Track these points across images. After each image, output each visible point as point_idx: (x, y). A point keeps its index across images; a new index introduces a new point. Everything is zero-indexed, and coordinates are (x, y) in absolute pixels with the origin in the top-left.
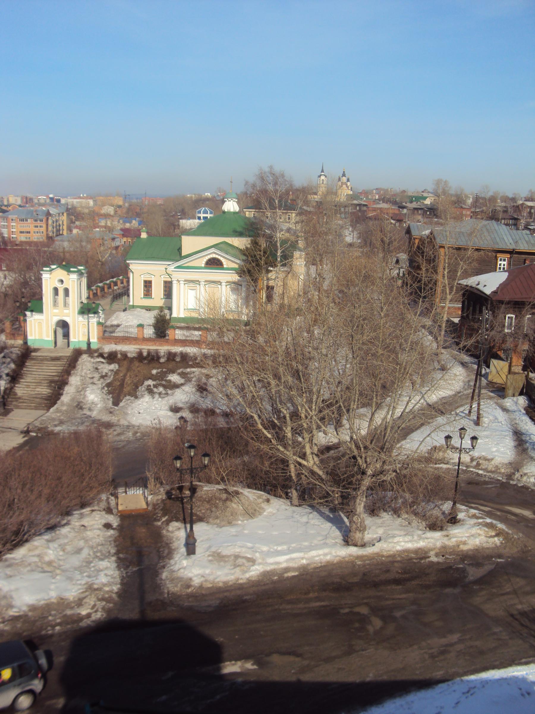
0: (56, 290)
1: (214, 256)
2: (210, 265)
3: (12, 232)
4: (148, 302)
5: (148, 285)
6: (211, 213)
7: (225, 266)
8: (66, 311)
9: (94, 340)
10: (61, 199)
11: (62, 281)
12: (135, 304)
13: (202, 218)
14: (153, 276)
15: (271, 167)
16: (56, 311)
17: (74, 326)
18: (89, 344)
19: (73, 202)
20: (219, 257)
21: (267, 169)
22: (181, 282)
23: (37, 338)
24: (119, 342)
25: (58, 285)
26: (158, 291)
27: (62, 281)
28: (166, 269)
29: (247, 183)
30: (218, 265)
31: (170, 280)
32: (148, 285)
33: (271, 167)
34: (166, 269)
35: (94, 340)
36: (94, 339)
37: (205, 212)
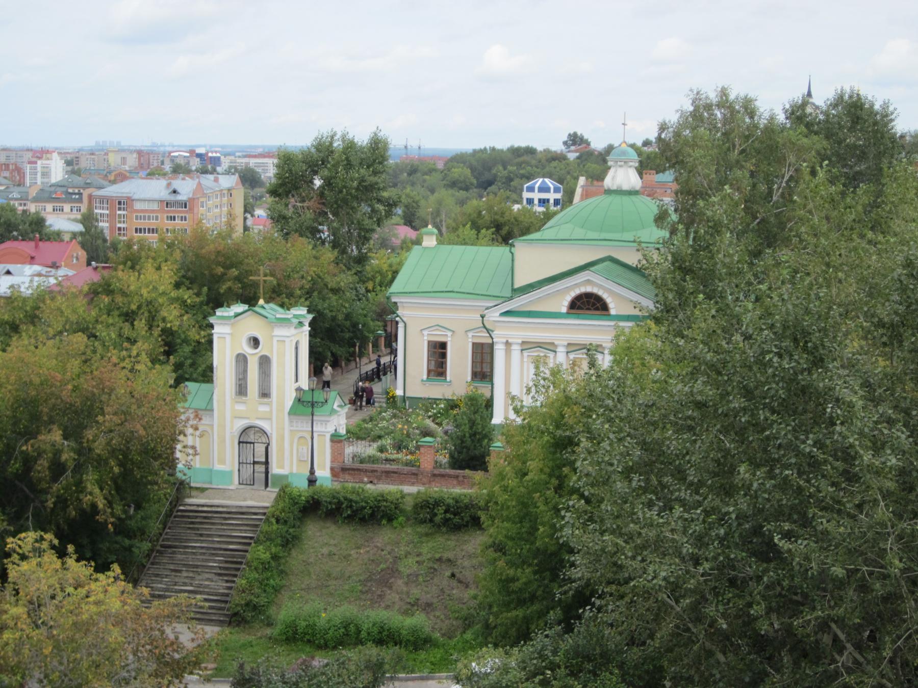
0: (242, 360)
1: (589, 289)
2: (579, 308)
3: (120, 229)
4: (437, 391)
5: (439, 351)
6: (557, 190)
7: (613, 312)
8: (263, 409)
9: (323, 473)
10: (222, 157)
11: (255, 342)
12: (407, 395)
13: (536, 202)
14: (449, 334)
15: (724, 93)
16: (240, 407)
17: (281, 438)
18: (312, 481)
19: (248, 163)
20: (600, 293)
21: (713, 97)
22: (514, 347)
23: (295, 471)
24: (379, 478)
25: (248, 350)
26: (460, 364)
27: (255, 342)
28: (483, 317)
29: (663, 127)
30: (597, 309)
31: (490, 341)
32: (439, 351)
33: (724, 93)
34: (483, 317)
35: (323, 473)
36: (324, 468)
37: (544, 189)
